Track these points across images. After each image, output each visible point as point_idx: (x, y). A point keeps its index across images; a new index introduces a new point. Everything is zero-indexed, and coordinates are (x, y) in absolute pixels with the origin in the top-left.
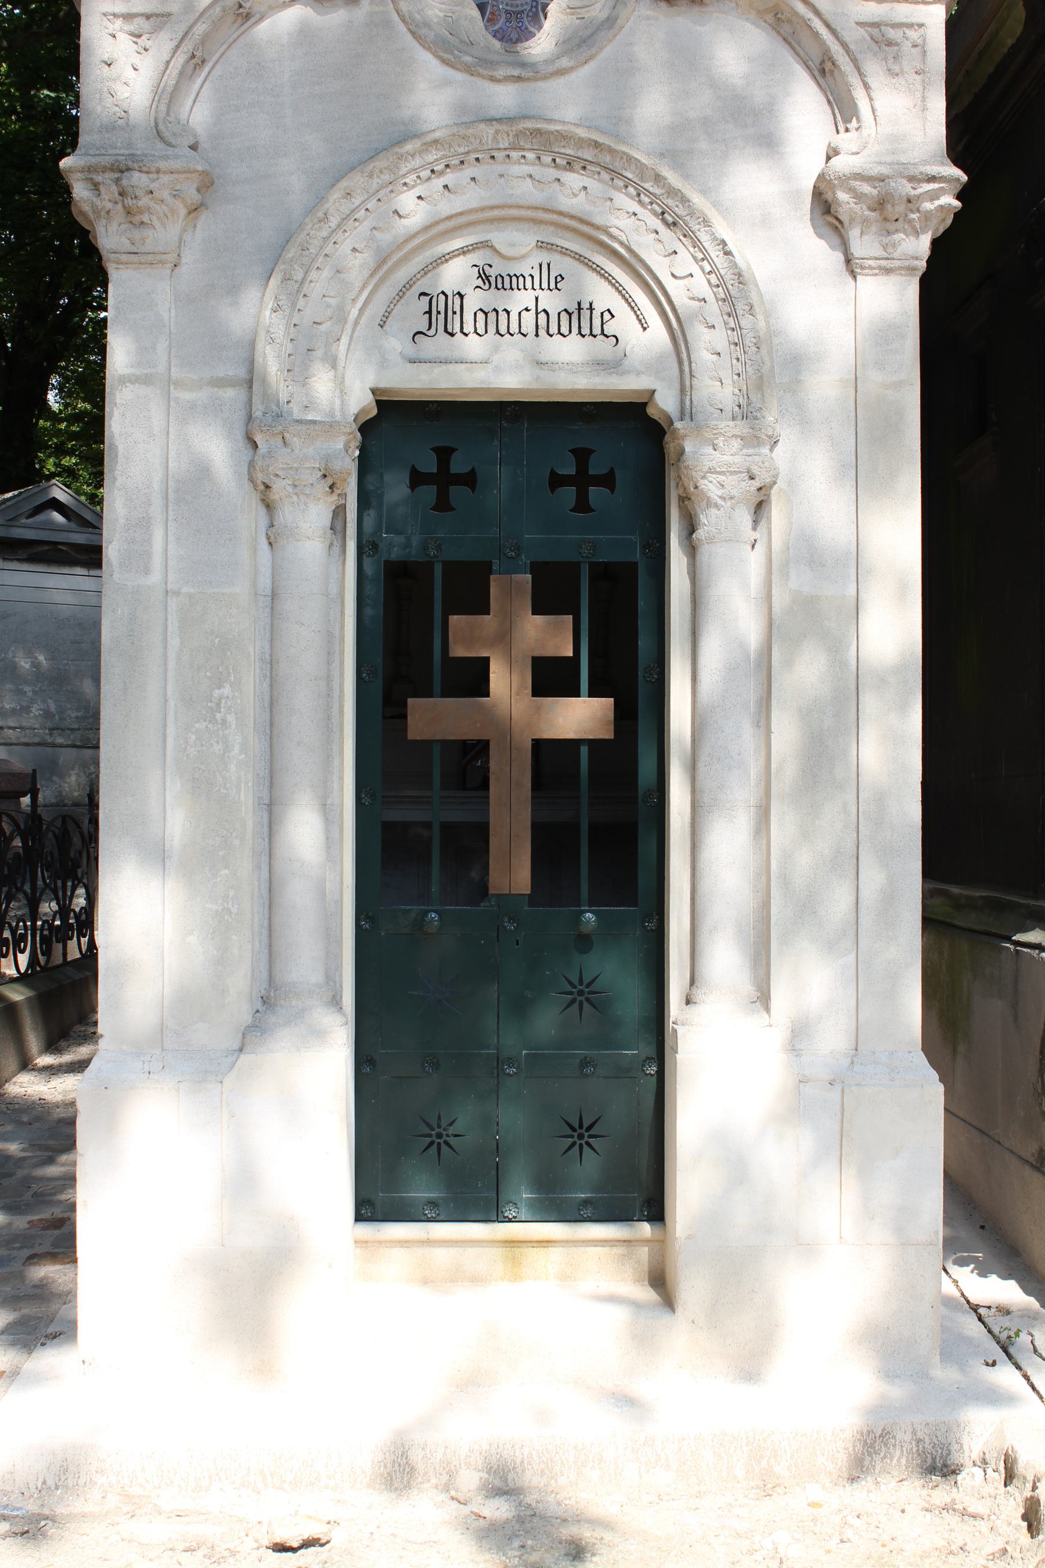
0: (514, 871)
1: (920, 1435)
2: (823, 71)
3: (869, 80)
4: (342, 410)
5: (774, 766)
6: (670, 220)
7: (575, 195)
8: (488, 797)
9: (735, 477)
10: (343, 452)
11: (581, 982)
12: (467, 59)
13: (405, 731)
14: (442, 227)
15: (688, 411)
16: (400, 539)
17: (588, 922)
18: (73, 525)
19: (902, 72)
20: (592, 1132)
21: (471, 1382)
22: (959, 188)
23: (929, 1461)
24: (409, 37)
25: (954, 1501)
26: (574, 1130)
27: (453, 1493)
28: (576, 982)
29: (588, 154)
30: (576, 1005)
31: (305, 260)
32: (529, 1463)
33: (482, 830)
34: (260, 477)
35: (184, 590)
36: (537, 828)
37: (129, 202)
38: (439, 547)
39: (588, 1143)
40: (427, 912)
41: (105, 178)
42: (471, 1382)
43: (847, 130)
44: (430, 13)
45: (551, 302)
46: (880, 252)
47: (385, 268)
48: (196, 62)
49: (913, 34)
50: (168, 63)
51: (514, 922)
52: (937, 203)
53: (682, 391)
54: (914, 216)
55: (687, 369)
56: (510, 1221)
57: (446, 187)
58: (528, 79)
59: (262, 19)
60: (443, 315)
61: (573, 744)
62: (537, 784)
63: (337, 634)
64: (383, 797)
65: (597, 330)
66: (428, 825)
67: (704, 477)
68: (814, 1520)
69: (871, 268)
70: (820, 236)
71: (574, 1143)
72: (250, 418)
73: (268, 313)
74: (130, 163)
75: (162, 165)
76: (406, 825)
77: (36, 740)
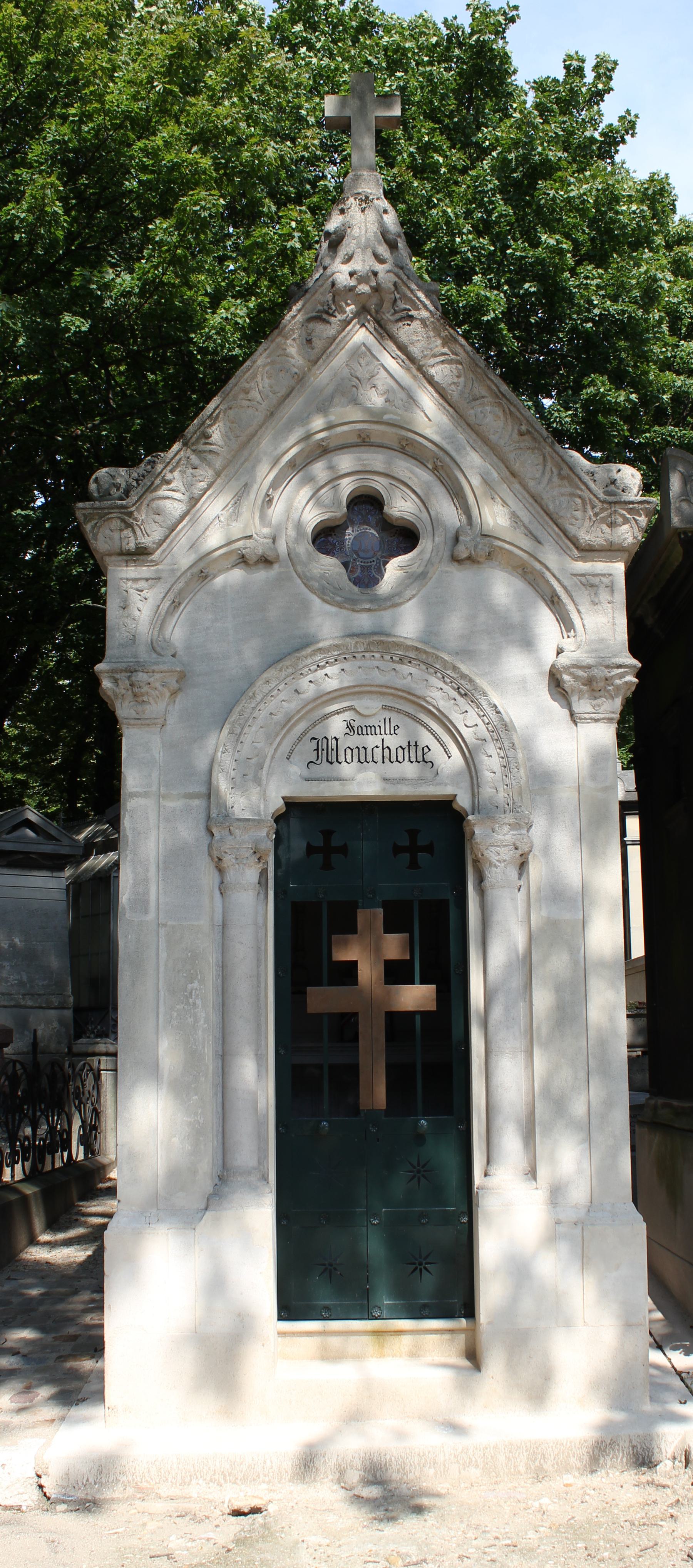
0: (376, 1092)
1: (634, 1443)
2: (553, 602)
3: (580, 608)
4: (265, 811)
5: (534, 1025)
6: (463, 692)
7: (405, 678)
8: (358, 1047)
9: (506, 848)
10: (265, 836)
11: (419, 1165)
12: (338, 599)
14: (324, 698)
15: (476, 808)
17: (422, 1126)
18: (41, 839)
19: (600, 602)
21: (355, 1417)
22: (636, 671)
23: (641, 1459)
24: (303, 586)
25: (653, 1480)
27: (343, 1484)
29: (412, 655)
30: (416, 1179)
31: (242, 722)
32: (390, 1465)
33: (354, 1069)
34: (215, 854)
35: (169, 923)
36: (389, 1067)
37: (136, 690)
40: (320, 1122)
41: (121, 676)
42: (355, 1417)
43: (568, 637)
44: (315, 571)
45: (393, 742)
46: (591, 710)
47: (290, 724)
48: (176, 604)
49: (606, 580)
50: (159, 606)
52: (624, 680)
53: (473, 795)
54: (611, 688)
55: (475, 782)
56: (376, 1319)
57: (326, 675)
58: (375, 610)
59: (215, 577)
60: (325, 751)
61: (410, 1015)
63: (263, 948)
65: (420, 759)
67: (487, 849)
68: (567, 1493)
69: (586, 719)
70: (554, 700)
71: (416, 1268)
72: (209, 818)
73: (219, 754)
74: (137, 667)
75: (155, 668)
77: (12, 1003)
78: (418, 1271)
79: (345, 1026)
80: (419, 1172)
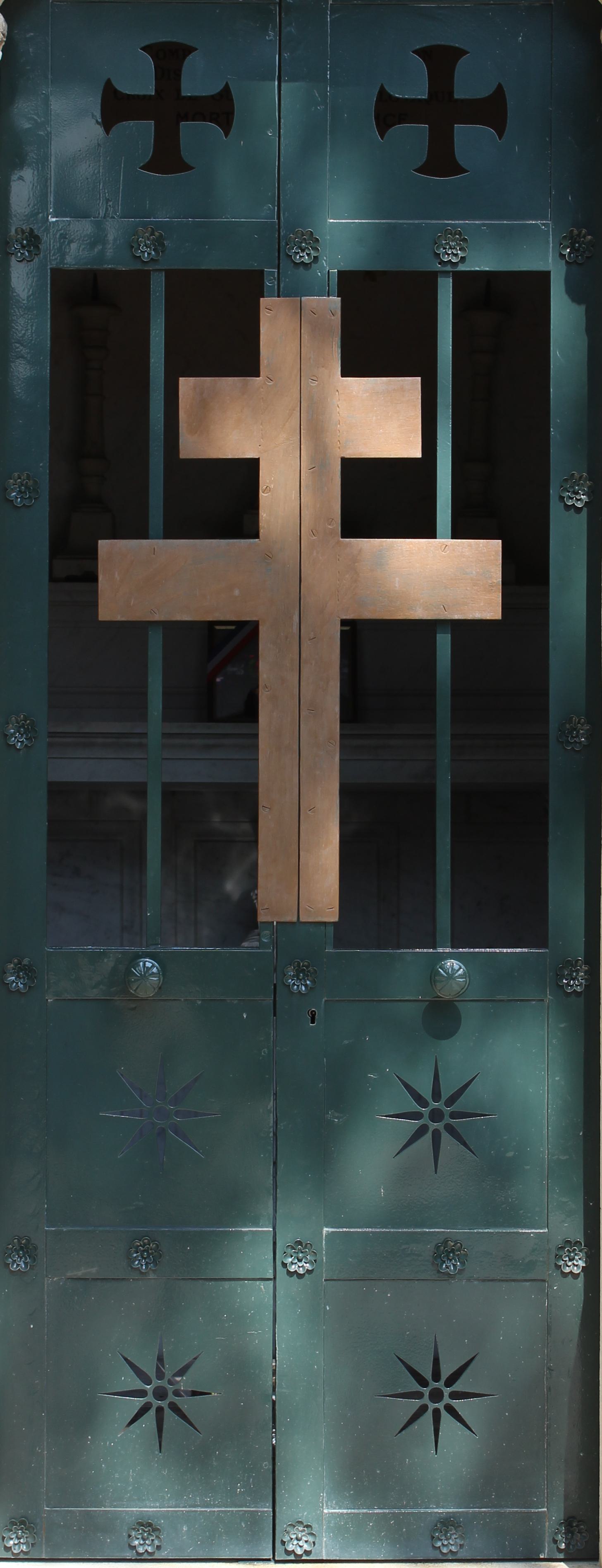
0: (308, 868)
8: (256, 736)
11: (436, 1095)
13: (95, 605)
16: (83, 228)
17: (451, 976)
20: (458, 1387)
26: (423, 1383)
28: (427, 1094)
33: (244, 799)
36: (350, 795)
38: (159, 245)
39: (450, 1409)
40: (138, 956)
51: (306, 976)
56: (298, 1560)
62: (353, 709)
64: (51, 735)
66: (139, 791)
71: (423, 1409)
76: (97, 791)
78: (414, 1106)
79: (218, 665)
80: (436, 1115)
